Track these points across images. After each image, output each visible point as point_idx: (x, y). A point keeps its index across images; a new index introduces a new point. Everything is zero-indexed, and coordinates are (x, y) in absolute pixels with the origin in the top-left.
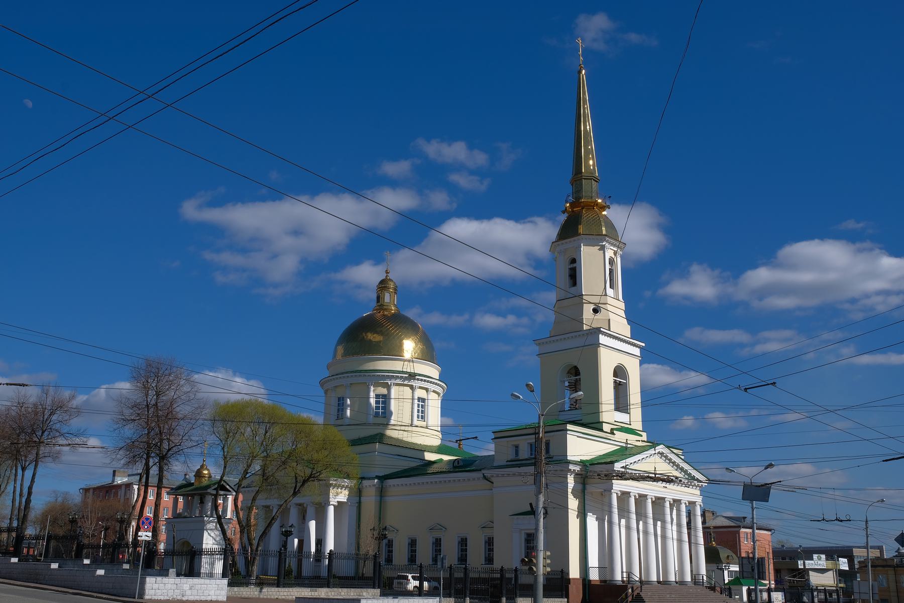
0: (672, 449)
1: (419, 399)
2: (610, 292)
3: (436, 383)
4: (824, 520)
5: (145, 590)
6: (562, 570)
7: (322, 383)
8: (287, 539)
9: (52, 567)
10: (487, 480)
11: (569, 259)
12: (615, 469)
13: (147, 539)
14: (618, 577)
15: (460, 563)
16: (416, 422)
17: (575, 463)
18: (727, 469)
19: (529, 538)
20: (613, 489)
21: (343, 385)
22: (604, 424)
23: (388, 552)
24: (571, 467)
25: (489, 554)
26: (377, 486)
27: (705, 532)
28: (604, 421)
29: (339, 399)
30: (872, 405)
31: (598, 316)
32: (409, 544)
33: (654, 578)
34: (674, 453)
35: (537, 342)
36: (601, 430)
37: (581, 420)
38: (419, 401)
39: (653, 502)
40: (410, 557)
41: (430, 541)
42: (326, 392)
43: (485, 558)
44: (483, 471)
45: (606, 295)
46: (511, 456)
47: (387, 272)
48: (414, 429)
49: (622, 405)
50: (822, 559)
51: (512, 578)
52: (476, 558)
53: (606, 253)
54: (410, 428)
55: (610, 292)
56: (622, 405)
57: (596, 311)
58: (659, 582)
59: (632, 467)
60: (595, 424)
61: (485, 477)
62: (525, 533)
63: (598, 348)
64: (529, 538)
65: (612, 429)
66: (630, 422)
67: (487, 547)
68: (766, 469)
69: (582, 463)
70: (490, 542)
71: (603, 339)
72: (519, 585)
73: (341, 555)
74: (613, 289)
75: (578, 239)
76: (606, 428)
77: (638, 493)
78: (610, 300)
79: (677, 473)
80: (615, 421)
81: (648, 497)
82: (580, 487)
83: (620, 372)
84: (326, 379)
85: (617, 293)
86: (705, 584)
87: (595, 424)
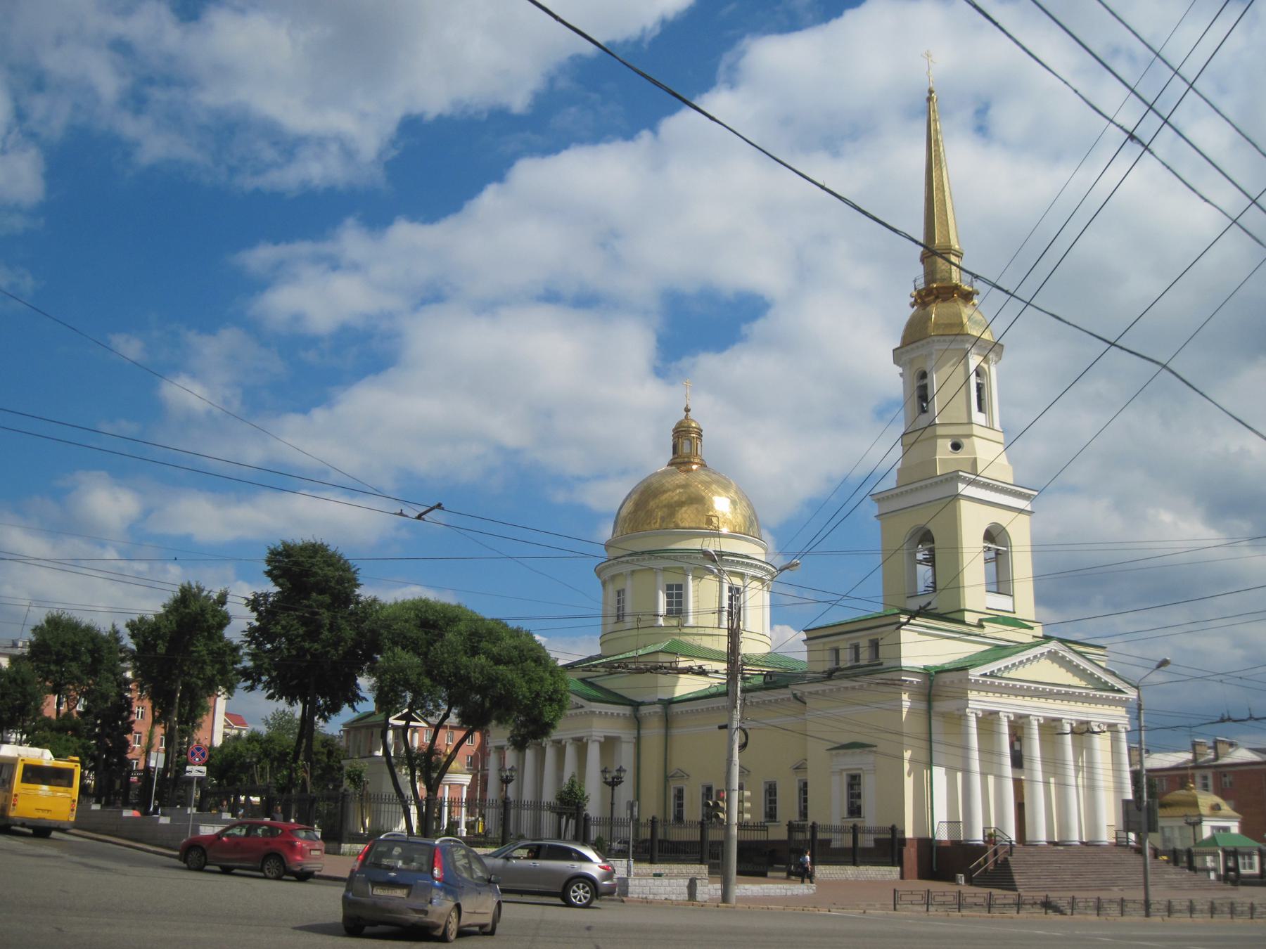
0: (1069, 645)
2: (978, 417)
4: (1251, 718)
7: (599, 571)
9: (223, 818)
11: (916, 374)
12: (970, 677)
13: (200, 775)
14: (1075, 837)
15: (803, 818)
17: (911, 672)
19: (854, 782)
20: (968, 707)
21: (622, 574)
22: (966, 613)
23: (770, 803)
25: (771, 809)
26: (660, 714)
27: (220, 641)
28: (967, 607)
29: (619, 592)
31: (960, 455)
32: (703, 794)
34: (1073, 650)
36: (963, 622)
40: (768, 810)
42: (604, 584)
43: (766, 812)
45: (970, 423)
46: (829, 665)
49: (1000, 582)
50: (619, 845)
55: (978, 417)
56: (1000, 582)
57: (956, 447)
59: (1013, 674)
60: (953, 616)
61: (795, 696)
63: (958, 503)
64: (854, 782)
65: (981, 620)
66: (1014, 609)
67: (768, 798)
70: (804, 789)
71: (963, 489)
73: (491, 802)
74: (985, 413)
75: (928, 343)
76: (970, 618)
78: (976, 430)
79: (1075, 681)
80: (988, 608)
81: (1001, 714)
82: (922, 706)
83: (993, 535)
84: (603, 565)
85: (991, 419)
87: (953, 616)
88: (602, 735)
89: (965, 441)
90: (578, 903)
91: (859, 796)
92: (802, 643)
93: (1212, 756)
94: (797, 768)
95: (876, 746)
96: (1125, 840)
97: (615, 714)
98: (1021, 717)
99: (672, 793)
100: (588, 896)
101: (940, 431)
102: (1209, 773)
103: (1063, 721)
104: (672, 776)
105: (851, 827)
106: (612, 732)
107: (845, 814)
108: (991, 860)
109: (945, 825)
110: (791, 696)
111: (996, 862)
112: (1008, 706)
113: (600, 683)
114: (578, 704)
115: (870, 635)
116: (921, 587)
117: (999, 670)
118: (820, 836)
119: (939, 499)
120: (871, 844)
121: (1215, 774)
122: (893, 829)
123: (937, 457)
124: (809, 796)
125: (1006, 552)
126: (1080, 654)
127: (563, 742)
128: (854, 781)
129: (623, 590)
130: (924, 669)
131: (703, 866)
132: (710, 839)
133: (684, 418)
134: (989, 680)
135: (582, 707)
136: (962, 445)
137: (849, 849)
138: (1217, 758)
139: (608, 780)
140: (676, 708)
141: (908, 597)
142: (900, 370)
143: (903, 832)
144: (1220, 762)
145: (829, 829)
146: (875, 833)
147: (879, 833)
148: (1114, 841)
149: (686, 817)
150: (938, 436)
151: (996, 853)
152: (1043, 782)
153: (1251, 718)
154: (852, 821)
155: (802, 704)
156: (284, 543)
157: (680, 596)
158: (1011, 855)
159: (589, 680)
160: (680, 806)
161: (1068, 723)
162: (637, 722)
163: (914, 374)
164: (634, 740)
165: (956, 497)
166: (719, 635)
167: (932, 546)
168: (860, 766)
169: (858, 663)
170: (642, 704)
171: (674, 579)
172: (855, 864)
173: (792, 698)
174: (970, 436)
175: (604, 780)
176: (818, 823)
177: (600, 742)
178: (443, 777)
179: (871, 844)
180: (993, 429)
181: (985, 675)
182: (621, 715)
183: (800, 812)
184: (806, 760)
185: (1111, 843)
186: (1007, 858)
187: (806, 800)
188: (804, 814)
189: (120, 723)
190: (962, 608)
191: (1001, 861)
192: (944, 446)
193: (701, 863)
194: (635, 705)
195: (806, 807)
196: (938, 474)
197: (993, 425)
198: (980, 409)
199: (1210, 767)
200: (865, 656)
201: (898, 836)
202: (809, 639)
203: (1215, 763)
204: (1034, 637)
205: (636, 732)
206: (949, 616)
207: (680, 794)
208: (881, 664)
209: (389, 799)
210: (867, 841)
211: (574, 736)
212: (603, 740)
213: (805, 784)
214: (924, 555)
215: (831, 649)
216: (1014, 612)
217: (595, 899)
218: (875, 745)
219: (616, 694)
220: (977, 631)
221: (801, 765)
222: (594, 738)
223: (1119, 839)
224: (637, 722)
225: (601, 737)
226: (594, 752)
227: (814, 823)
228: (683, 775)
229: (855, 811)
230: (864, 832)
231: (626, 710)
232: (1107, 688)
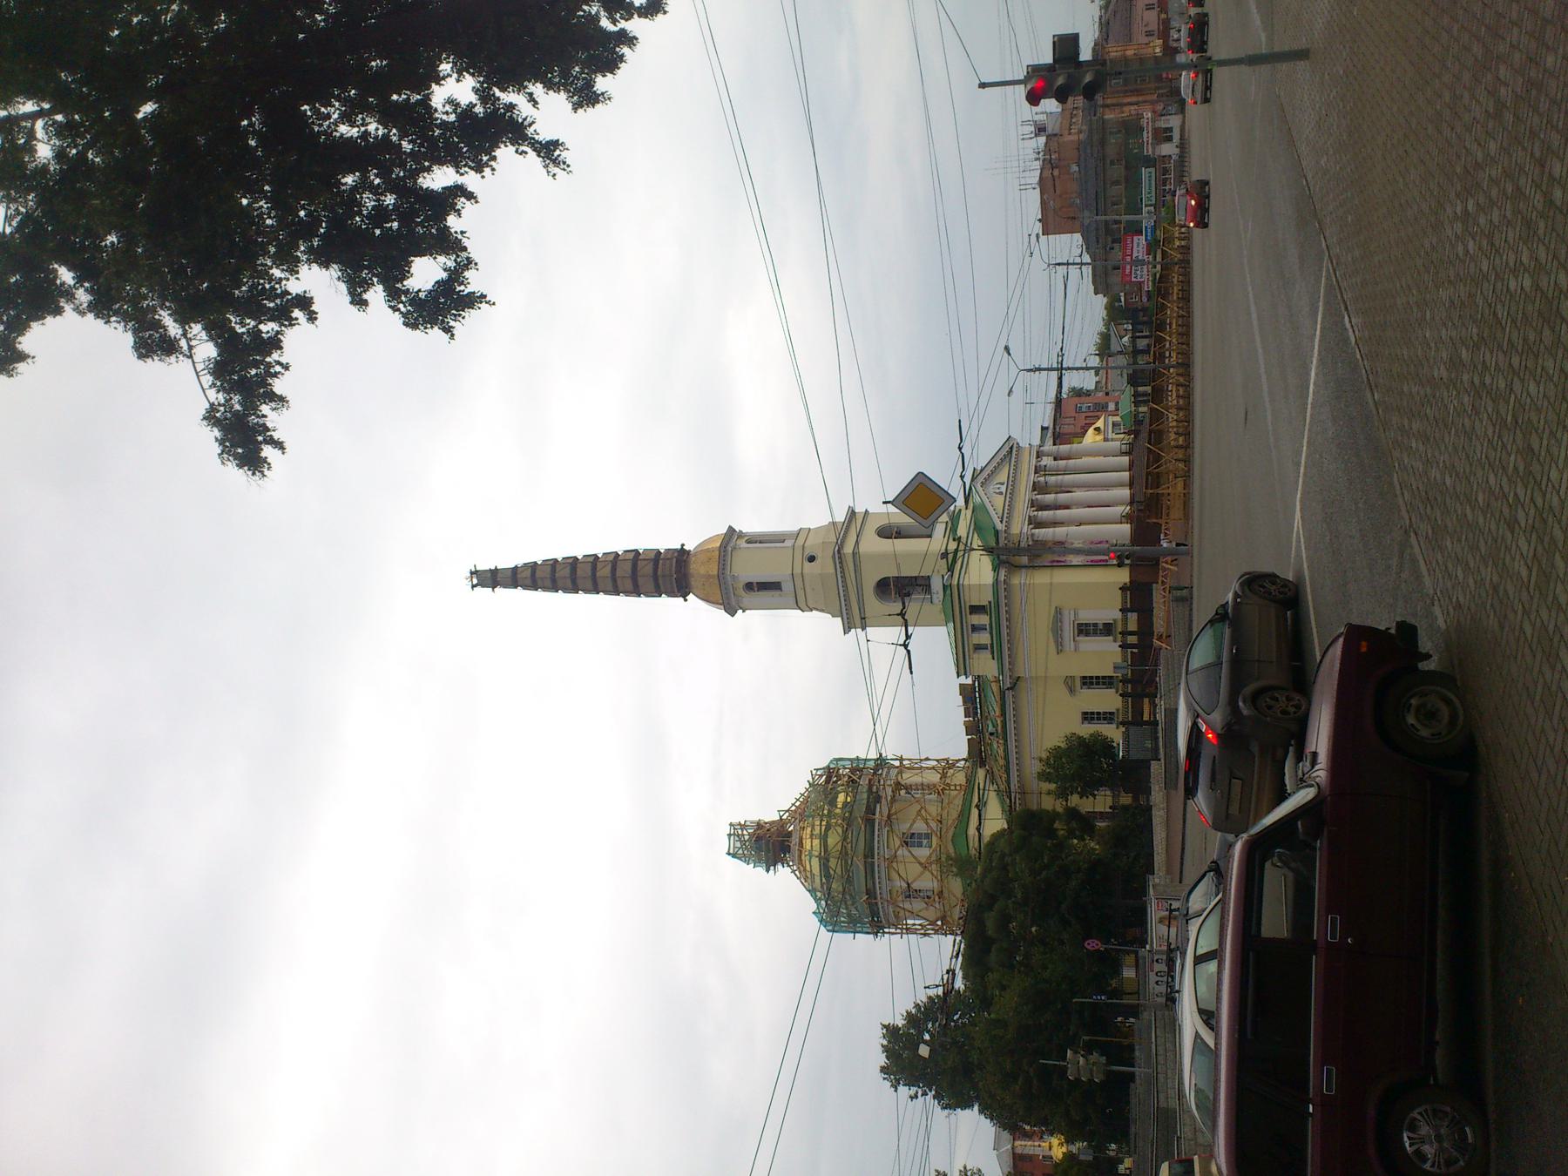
4: (905, 646)
5: (1128, 1103)
6: (1120, 589)
18: (1009, 395)
25: (1104, 684)
30: (938, 206)
31: (819, 555)
35: (847, 631)
40: (1106, 722)
43: (1107, 688)
51: (1131, 652)
52: (1109, 700)
53: (630, 571)
57: (812, 559)
58: (1130, 470)
65: (954, 540)
67: (1095, 686)
69: (996, 569)
70: (1088, 682)
86: (1039, 464)
89: (808, 552)
91: (1095, 625)
107: (1111, 638)
112: (1022, 509)
128: (1084, 630)
130: (995, 571)
133: (784, 876)
134: (1005, 519)
142: (740, 611)
152: (1051, 584)
156: (1052, 222)
169: (988, 627)
181: (1001, 522)
189: (301, 36)
200: (982, 619)
202: (965, 674)
208: (990, 602)
229: (1108, 629)
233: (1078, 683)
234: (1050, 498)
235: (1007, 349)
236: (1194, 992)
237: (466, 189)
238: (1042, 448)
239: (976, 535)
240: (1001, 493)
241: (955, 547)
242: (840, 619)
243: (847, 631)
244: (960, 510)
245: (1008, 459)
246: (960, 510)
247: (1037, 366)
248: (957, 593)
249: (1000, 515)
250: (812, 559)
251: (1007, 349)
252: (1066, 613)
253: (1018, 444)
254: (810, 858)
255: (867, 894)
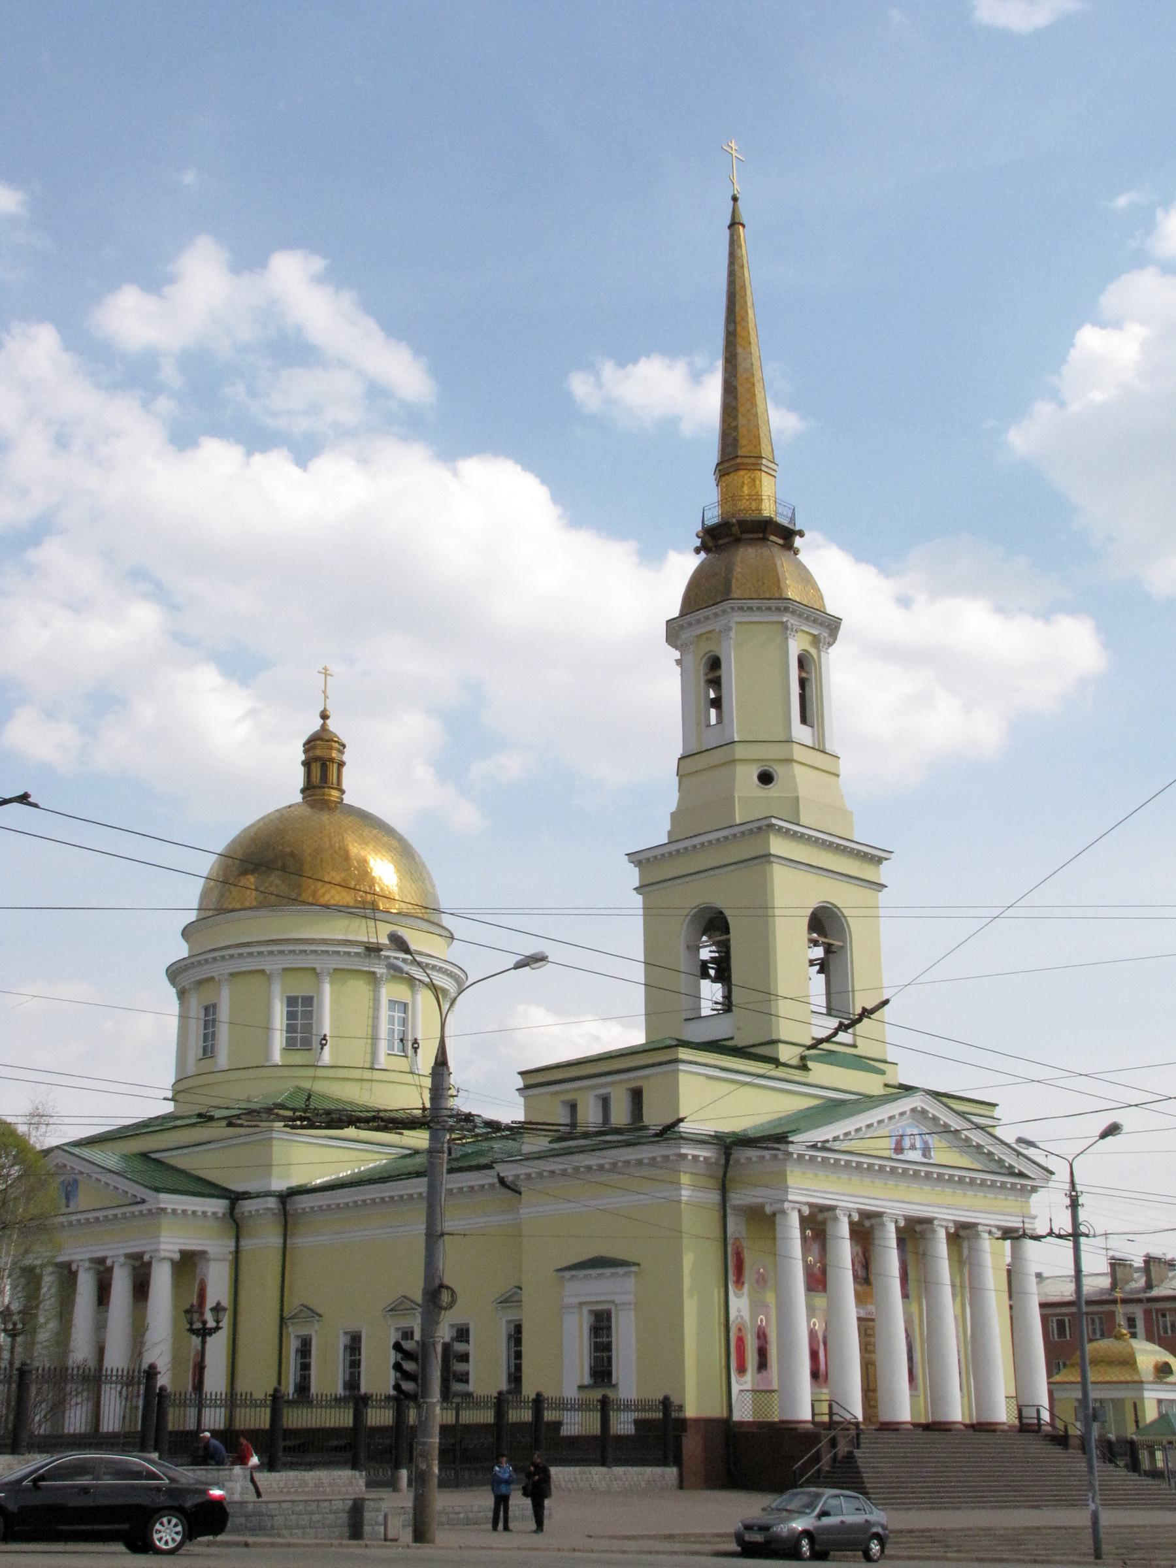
1: (392, 1003)
3: (447, 970)
8: (204, 1343)
10: (508, 1187)
11: (704, 659)
16: (383, 1060)
24: (688, 1150)
29: (206, 1009)
31: (773, 791)
33: (1003, 1413)
34: (949, 1107)
36: (775, 1062)
37: (732, 1038)
38: (391, 1009)
39: (949, 1236)
40: (513, 1369)
41: (503, 1332)
42: (182, 994)
44: (499, 1167)
47: (324, 716)
48: (377, 1075)
54: (367, 1074)
55: (801, 733)
57: (766, 778)
61: (502, 1181)
62: (591, 1311)
68: (518, 966)
70: (516, 1336)
71: (778, 846)
72: (171, 1433)
76: (786, 1054)
77: (903, 1215)
78: (798, 753)
81: (980, 1228)
88: (177, 1248)
89: (779, 770)
90: (164, 1547)
92: (517, 1093)
93: (1142, 1282)
94: (505, 1301)
95: (638, 1265)
96: (1036, 1421)
97: (179, 1212)
98: (866, 1215)
99: (293, 1345)
100: (178, 1538)
101: (740, 752)
102: (1138, 1312)
103: (936, 1222)
104: (292, 1318)
105: (598, 1401)
106: (192, 1245)
107: (587, 1380)
108: (826, 1459)
109: (749, 1395)
110: (496, 1180)
111: (835, 1457)
113: (174, 1162)
114: (135, 1196)
115: (630, 1080)
116: (706, 1009)
117: (836, 1139)
118: (549, 1416)
119: (695, 873)
120: (630, 1429)
121: (1147, 1313)
122: (666, 1403)
123: (736, 795)
124: (525, 1348)
125: (842, 947)
126: (962, 1115)
127: (109, 1262)
128: (601, 1324)
129: (214, 1006)
131: (357, 1473)
132: (369, 1424)
135: (143, 1201)
136: (775, 777)
137: (595, 1438)
138: (1149, 1286)
139: (195, 1327)
140: (303, 1203)
141: (686, 1020)
142: (677, 655)
143: (681, 1408)
144: (1155, 1293)
145: (562, 1405)
146: (637, 1410)
147: (644, 1410)
148: (1016, 1422)
149: (314, 1389)
150: (738, 760)
151: (833, 1443)
153: (1051, 1233)
154: (597, 1394)
155: (515, 1194)
157: (308, 1015)
158: (858, 1447)
159: (153, 1156)
160: (305, 1367)
161: (942, 1226)
162: (234, 1226)
163: (702, 658)
164: (230, 1257)
165: (766, 857)
166: (372, 1080)
167: (724, 937)
168: (609, 1298)
170: (245, 1196)
171: (301, 988)
172: (603, 1462)
173: (498, 1185)
174: (790, 761)
175: (188, 1326)
176: (546, 1395)
177: (172, 1261)
178: (1146, 1276)
179: (630, 1429)
180: (824, 752)
182: (209, 1214)
183: (509, 1375)
184: (520, 1288)
185: (1011, 1426)
186: (851, 1452)
187: (518, 1355)
188: (516, 1377)
190: (774, 1037)
191: (843, 1457)
192: (747, 775)
193: (355, 1466)
194: (235, 1198)
195: (518, 1368)
196: (738, 822)
197: (824, 744)
198: (804, 720)
199: (1139, 1301)
200: (620, 1115)
201: (674, 1415)
202: (527, 1087)
203: (1148, 1295)
204: (886, 1085)
205: (232, 1243)
206: (753, 1050)
207: (305, 1350)
209: (327, 1401)
210: (623, 1424)
211: (130, 1251)
212: (177, 1256)
213: (518, 1329)
214: (711, 952)
215: (564, 1103)
216: (854, 1046)
217: (188, 1540)
218: (635, 1260)
219: (200, 1179)
220: (798, 1075)
221: (510, 1296)
222: (163, 1254)
223: (1025, 1421)
224: (235, 1223)
225: (175, 1252)
226: (162, 1280)
227: (539, 1395)
228: (312, 1314)
229: (602, 1372)
230: (619, 1409)
231: (218, 1206)
232: (1003, 1171)
233: (512, 1315)
234: (891, 1260)
235: (1113, 1130)
236: (183, 1145)
237: (371, 873)
238: (986, 1235)
239: (813, 1102)
240: (899, 1149)
241: (782, 1060)
242: (666, 841)
243: (635, 858)
244: (882, 1072)
245: (996, 1169)
246: (882, 1072)
247: (1081, 1200)
248: (650, 1061)
249: (836, 1145)
250: (766, 778)
251: (1113, 1130)
252: (630, 1284)
253: (1034, 1189)
254: (352, 1383)
255: (830, 1012)
